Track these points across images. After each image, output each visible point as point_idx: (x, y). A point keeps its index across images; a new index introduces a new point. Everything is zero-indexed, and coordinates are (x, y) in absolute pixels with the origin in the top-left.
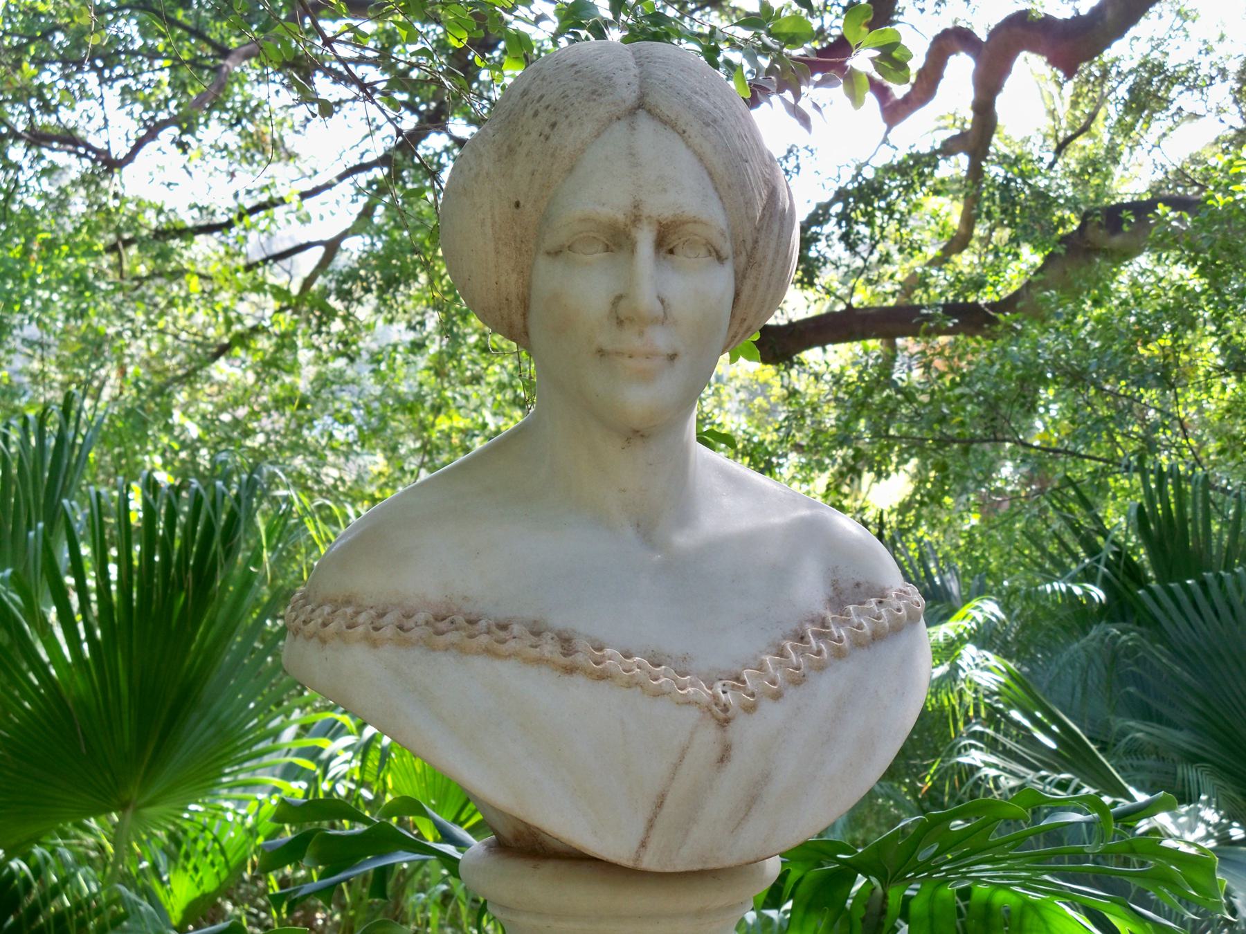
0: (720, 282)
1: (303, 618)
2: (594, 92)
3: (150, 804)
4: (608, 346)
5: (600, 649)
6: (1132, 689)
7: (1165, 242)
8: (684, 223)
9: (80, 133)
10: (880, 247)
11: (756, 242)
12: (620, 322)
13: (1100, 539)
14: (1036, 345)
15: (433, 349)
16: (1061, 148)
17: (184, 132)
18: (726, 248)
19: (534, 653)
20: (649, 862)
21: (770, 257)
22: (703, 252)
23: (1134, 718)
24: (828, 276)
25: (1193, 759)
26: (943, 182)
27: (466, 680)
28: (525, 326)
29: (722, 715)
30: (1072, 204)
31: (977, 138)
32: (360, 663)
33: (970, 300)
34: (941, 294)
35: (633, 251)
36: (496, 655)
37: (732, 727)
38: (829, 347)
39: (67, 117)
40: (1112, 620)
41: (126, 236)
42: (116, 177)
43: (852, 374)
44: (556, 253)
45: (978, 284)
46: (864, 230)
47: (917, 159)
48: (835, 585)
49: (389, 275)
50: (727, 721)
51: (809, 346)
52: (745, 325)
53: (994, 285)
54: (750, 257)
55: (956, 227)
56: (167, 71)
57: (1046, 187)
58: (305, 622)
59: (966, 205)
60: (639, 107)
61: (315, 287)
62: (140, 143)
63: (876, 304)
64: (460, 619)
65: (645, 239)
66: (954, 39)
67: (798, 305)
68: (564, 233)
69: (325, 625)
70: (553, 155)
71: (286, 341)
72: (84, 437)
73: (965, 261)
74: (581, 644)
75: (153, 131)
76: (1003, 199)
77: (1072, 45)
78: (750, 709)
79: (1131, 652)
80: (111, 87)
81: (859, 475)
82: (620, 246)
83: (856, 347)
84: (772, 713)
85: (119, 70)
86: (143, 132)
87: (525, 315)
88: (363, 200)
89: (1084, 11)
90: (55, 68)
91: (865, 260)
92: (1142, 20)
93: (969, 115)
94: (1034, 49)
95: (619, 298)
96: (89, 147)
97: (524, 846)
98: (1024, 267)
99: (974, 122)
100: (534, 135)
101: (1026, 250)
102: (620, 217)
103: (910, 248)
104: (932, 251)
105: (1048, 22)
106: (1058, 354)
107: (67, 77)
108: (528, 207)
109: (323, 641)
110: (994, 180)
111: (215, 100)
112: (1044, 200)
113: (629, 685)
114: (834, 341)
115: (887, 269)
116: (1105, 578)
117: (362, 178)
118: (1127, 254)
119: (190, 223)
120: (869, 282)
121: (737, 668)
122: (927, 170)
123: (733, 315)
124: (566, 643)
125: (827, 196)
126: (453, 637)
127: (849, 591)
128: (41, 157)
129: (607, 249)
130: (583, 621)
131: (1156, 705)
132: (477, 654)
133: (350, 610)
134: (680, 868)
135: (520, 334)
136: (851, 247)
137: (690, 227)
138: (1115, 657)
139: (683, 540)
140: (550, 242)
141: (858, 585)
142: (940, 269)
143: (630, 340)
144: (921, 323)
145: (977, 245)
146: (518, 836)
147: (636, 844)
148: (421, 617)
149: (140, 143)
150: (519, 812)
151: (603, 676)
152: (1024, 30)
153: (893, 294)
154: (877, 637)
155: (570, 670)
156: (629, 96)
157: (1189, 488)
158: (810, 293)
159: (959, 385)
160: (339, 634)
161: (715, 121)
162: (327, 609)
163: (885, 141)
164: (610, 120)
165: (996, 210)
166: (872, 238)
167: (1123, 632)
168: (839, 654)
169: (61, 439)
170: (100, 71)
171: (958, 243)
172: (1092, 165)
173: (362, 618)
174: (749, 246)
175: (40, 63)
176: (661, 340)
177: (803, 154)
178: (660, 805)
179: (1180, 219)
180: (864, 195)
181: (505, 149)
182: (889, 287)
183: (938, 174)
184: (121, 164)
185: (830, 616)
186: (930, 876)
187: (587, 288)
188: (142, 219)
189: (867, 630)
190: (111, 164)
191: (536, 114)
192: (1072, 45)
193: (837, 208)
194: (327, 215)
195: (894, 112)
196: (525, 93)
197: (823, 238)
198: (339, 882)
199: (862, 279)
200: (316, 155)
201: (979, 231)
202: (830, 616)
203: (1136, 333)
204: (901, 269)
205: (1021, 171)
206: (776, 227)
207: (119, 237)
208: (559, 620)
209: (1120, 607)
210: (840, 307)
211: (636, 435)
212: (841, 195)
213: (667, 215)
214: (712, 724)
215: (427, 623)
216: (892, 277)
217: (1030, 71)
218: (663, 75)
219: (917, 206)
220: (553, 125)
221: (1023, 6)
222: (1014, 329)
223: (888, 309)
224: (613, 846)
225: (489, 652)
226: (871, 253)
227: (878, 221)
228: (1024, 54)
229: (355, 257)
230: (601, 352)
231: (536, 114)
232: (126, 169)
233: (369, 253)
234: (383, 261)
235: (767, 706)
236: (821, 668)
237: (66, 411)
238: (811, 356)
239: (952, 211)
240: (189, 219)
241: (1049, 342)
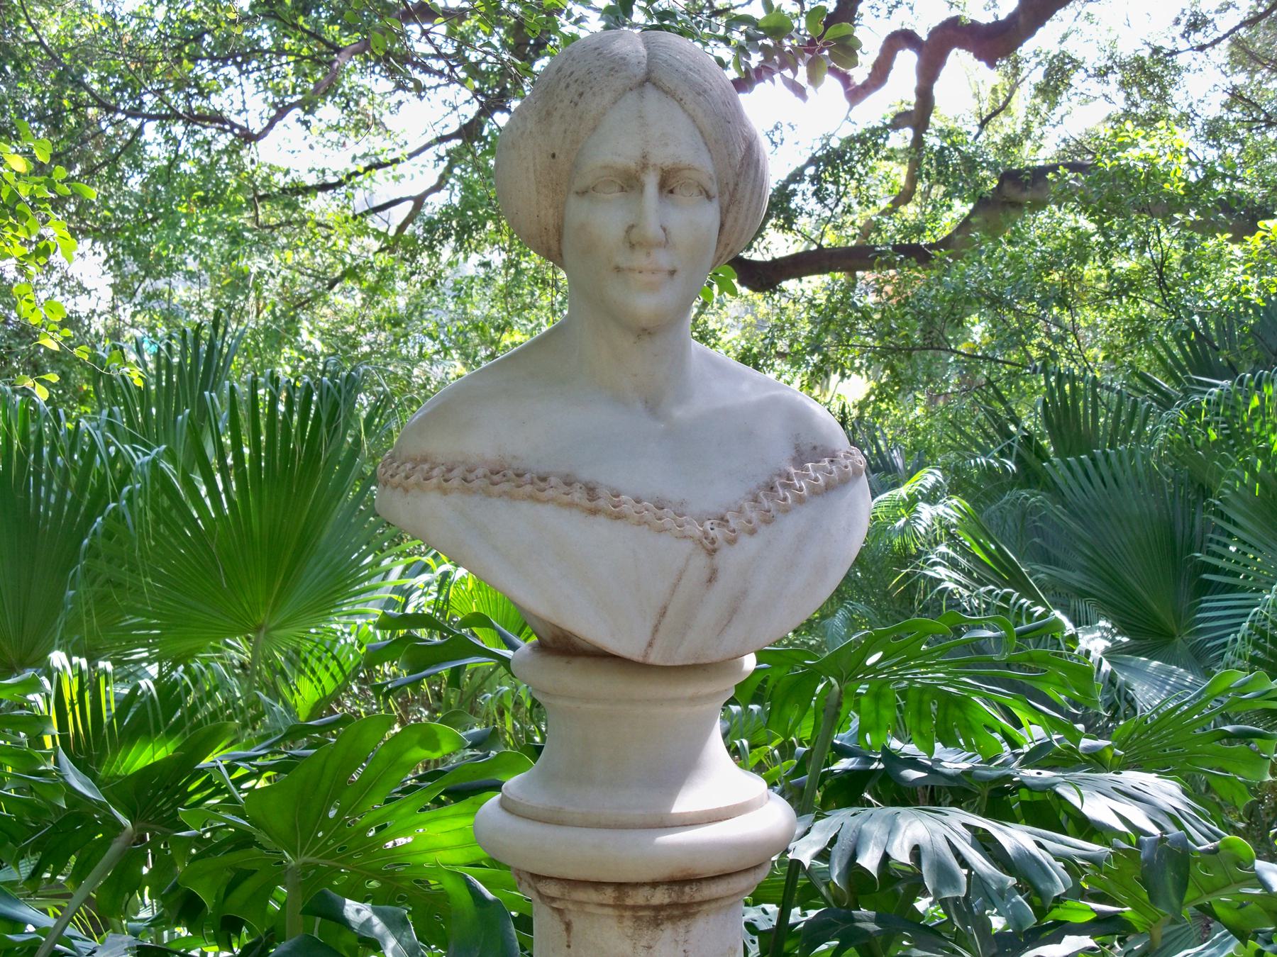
0: (709, 215)
1: (390, 472)
2: (612, 69)
3: (279, 627)
4: (623, 264)
5: (617, 496)
6: (1037, 540)
7: (1063, 198)
8: (680, 170)
9: (225, 114)
10: (844, 200)
11: (737, 185)
12: (632, 246)
13: (1012, 428)
14: (964, 275)
15: (500, 281)
16: (983, 124)
17: (307, 113)
18: (714, 190)
19: (567, 498)
20: (655, 658)
21: (748, 196)
22: (696, 191)
23: (1036, 562)
24: (802, 222)
25: (1083, 594)
26: (892, 150)
27: (517, 520)
28: (560, 249)
29: (710, 547)
30: (993, 166)
31: (919, 116)
32: (433, 508)
33: (914, 241)
34: (891, 237)
35: (642, 191)
36: (538, 500)
37: (718, 556)
38: (805, 279)
39: (216, 102)
40: (1021, 487)
41: (261, 193)
42: (253, 148)
43: (821, 299)
44: (583, 193)
45: (920, 229)
46: (831, 188)
47: (874, 131)
48: (797, 448)
49: (463, 225)
50: (714, 551)
51: (787, 278)
52: (729, 249)
53: (932, 230)
54: (732, 195)
55: (903, 184)
56: (292, 65)
57: (974, 153)
58: (392, 476)
59: (910, 168)
60: (648, 80)
61: (406, 233)
62: (272, 122)
63: (842, 244)
64: (510, 473)
65: (651, 182)
66: (904, 38)
67: (776, 244)
68: (584, 171)
69: (407, 478)
70: (580, 118)
71: (385, 275)
72: (229, 346)
73: (910, 212)
74: (603, 492)
75: (282, 111)
76: (939, 164)
77: (995, 42)
78: (732, 542)
79: (1035, 509)
80: (248, 78)
81: (827, 375)
82: (632, 187)
83: (827, 278)
84: (748, 545)
85: (255, 64)
86: (273, 113)
87: (559, 241)
88: (444, 164)
89: (1002, 17)
90: (205, 63)
91: (832, 210)
92: (1048, 23)
93: (913, 99)
94: (962, 45)
95: (632, 227)
96: (233, 126)
97: (561, 646)
98: (956, 216)
99: (917, 105)
100: (567, 102)
101: (957, 203)
102: (632, 165)
103: (869, 202)
104: (884, 204)
105: (974, 26)
106: (981, 283)
107: (214, 70)
108: (561, 157)
109: (406, 490)
110: (932, 148)
111: (329, 88)
112: (970, 163)
113: (639, 524)
114: (807, 275)
115: (849, 218)
116: (1018, 455)
117: (442, 149)
118: (1039, 205)
119: (309, 184)
120: (836, 228)
121: (722, 511)
122: (881, 141)
123: (719, 241)
124: (591, 491)
125: (804, 161)
126: (505, 486)
127: (809, 451)
128: (195, 132)
129: (622, 189)
131: (1053, 551)
132: (524, 499)
133: (426, 467)
134: (680, 663)
135: (554, 255)
136: (821, 200)
137: (686, 173)
138: (1024, 516)
139: (679, 413)
140: (579, 184)
141: (815, 448)
142: (890, 218)
143: (639, 259)
144: (875, 258)
145: (919, 199)
146: (555, 639)
147: (644, 644)
148: (480, 472)
149: (272, 122)
150: (556, 621)
151: (619, 517)
152: (955, 33)
153: (854, 237)
154: (829, 487)
155: (594, 512)
156: (640, 72)
157: (1082, 385)
158: (790, 235)
159: (904, 305)
160: (417, 484)
161: (705, 91)
162: (409, 466)
163: (847, 118)
164: (625, 91)
165: (933, 171)
166: (838, 193)
167: (1033, 495)
168: (800, 500)
169: (212, 346)
170: (239, 65)
171: (904, 197)
172: (1013, 141)
173: (435, 472)
174: (731, 187)
175: (194, 58)
176: (663, 259)
177: (786, 128)
178: (663, 614)
179: (1076, 179)
180: (833, 161)
181: (544, 113)
182: (851, 232)
183: (889, 145)
184: (257, 138)
185: (793, 471)
186: (875, 677)
187: (606, 220)
188: (274, 179)
189: (821, 482)
190: (248, 137)
191: (567, 86)
192: (995, 42)
193: (810, 171)
194: (417, 175)
195: (856, 94)
196: (559, 70)
197: (800, 194)
198: (421, 679)
199: (829, 226)
200: (405, 131)
201: (920, 187)
202: (793, 471)
203: (1041, 267)
204: (861, 216)
205: (953, 142)
206: (752, 173)
207: (256, 195)
208: (586, 474)
209: (1030, 476)
210: (814, 247)
211: (645, 332)
212: (813, 161)
213: (668, 163)
214: (703, 553)
215: (485, 476)
216: (853, 223)
217: (960, 61)
218: (666, 57)
219: (872, 169)
220: (581, 95)
221: (955, 12)
222: (947, 262)
223: (852, 248)
225: (532, 498)
226: (837, 205)
227: (842, 181)
228: (955, 50)
229: (437, 210)
230: (618, 269)
231: (567, 86)
232: (260, 143)
233: (447, 207)
234: (459, 213)
235: (745, 540)
236: (786, 511)
237: (215, 326)
238: (790, 285)
239: (899, 173)
240: (311, 180)
241: (970, 272)
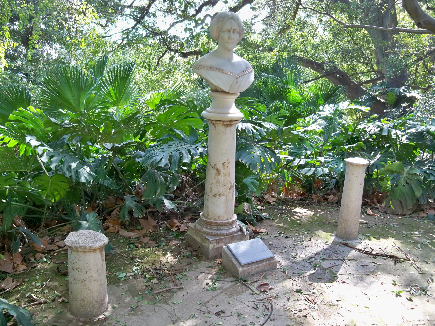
20: (230, 92)
44: (223, 32)
65: (232, 31)
84: (241, 78)
124: (222, 70)
130: (224, 69)
140: (222, 31)
151: (226, 74)
208: (222, 68)
224: (227, 90)
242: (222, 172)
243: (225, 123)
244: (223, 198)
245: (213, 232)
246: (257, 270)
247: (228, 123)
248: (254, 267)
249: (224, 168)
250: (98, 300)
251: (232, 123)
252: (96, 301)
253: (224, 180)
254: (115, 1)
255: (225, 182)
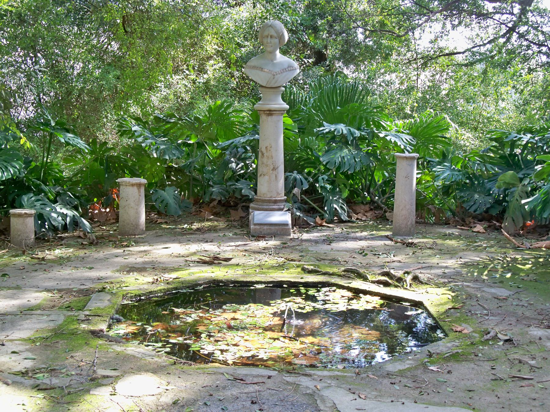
242: (265, 155)
243: (266, 112)
244: (267, 177)
245: (260, 207)
246: (269, 231)
247: (268, 112)
248: (265, 227)
249: (267, 151)
250: (134, 223)
251: (271, 112)
252: (132, 224)
253: (267, 162)
254: (549, 23)
255: (268, 163)
